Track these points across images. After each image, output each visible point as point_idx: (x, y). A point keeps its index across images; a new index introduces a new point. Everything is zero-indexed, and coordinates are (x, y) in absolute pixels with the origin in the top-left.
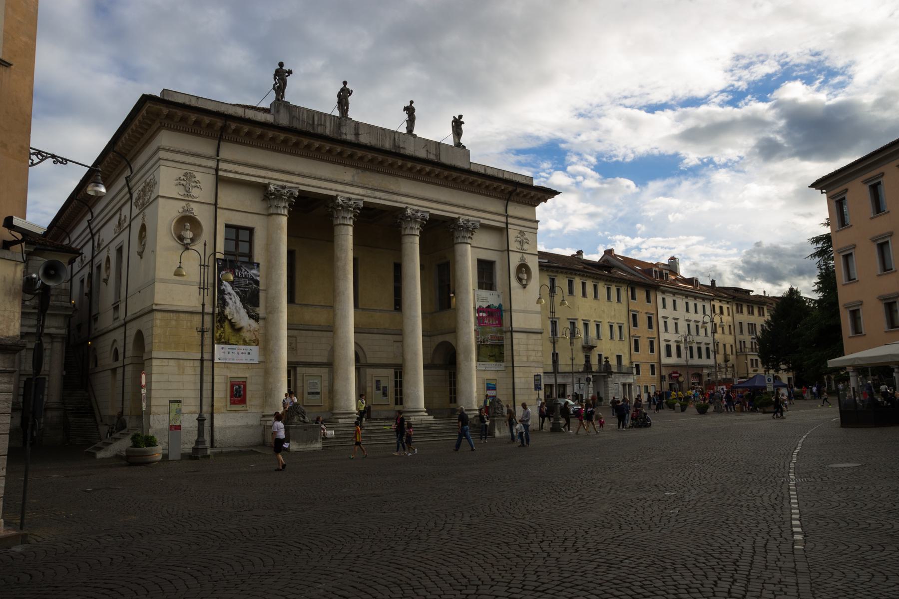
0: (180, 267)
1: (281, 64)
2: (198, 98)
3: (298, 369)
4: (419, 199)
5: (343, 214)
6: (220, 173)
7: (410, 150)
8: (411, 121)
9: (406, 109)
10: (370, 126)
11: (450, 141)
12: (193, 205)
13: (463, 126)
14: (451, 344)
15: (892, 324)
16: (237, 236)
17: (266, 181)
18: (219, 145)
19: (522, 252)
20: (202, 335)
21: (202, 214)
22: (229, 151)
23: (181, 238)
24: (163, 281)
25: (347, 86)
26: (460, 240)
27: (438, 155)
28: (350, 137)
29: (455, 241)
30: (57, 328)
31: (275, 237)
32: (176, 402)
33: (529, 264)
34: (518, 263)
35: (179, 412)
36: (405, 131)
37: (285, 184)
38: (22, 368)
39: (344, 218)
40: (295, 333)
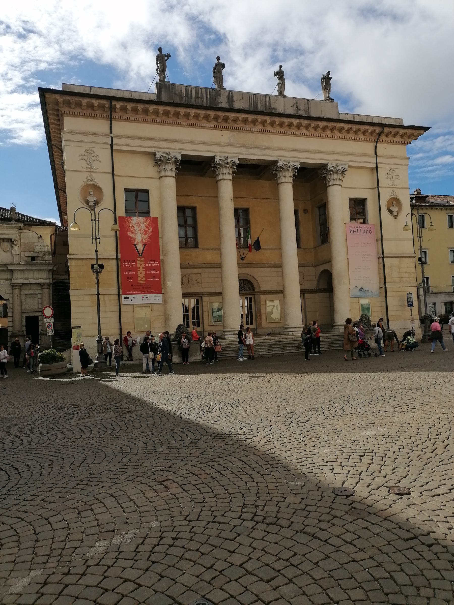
0: (406, 225)
2: (91, 87)
3: (203, 298)
4: (290, 149)
6: (114, 147)
8: (282, 85)
11: (322, 97)
12: (94, 175)
13: (331, 81)
14: (329, 271)
15: (451, 226)
16: (137, 197)
17: (152, 150)
18: (111, 124)
21: (105, 183)
22: (120, 127)
23: (87, 202)
24: (105, 237)
25: (220, 61)
26: (331, 183)
27: (354, 118)
29: (327, 185)
30: (43, 279)
31: (165, 196)
33: (100, 185)
34: (389, 198)
36: (276, 93)
38: (23, 307)
40: (302, 269)
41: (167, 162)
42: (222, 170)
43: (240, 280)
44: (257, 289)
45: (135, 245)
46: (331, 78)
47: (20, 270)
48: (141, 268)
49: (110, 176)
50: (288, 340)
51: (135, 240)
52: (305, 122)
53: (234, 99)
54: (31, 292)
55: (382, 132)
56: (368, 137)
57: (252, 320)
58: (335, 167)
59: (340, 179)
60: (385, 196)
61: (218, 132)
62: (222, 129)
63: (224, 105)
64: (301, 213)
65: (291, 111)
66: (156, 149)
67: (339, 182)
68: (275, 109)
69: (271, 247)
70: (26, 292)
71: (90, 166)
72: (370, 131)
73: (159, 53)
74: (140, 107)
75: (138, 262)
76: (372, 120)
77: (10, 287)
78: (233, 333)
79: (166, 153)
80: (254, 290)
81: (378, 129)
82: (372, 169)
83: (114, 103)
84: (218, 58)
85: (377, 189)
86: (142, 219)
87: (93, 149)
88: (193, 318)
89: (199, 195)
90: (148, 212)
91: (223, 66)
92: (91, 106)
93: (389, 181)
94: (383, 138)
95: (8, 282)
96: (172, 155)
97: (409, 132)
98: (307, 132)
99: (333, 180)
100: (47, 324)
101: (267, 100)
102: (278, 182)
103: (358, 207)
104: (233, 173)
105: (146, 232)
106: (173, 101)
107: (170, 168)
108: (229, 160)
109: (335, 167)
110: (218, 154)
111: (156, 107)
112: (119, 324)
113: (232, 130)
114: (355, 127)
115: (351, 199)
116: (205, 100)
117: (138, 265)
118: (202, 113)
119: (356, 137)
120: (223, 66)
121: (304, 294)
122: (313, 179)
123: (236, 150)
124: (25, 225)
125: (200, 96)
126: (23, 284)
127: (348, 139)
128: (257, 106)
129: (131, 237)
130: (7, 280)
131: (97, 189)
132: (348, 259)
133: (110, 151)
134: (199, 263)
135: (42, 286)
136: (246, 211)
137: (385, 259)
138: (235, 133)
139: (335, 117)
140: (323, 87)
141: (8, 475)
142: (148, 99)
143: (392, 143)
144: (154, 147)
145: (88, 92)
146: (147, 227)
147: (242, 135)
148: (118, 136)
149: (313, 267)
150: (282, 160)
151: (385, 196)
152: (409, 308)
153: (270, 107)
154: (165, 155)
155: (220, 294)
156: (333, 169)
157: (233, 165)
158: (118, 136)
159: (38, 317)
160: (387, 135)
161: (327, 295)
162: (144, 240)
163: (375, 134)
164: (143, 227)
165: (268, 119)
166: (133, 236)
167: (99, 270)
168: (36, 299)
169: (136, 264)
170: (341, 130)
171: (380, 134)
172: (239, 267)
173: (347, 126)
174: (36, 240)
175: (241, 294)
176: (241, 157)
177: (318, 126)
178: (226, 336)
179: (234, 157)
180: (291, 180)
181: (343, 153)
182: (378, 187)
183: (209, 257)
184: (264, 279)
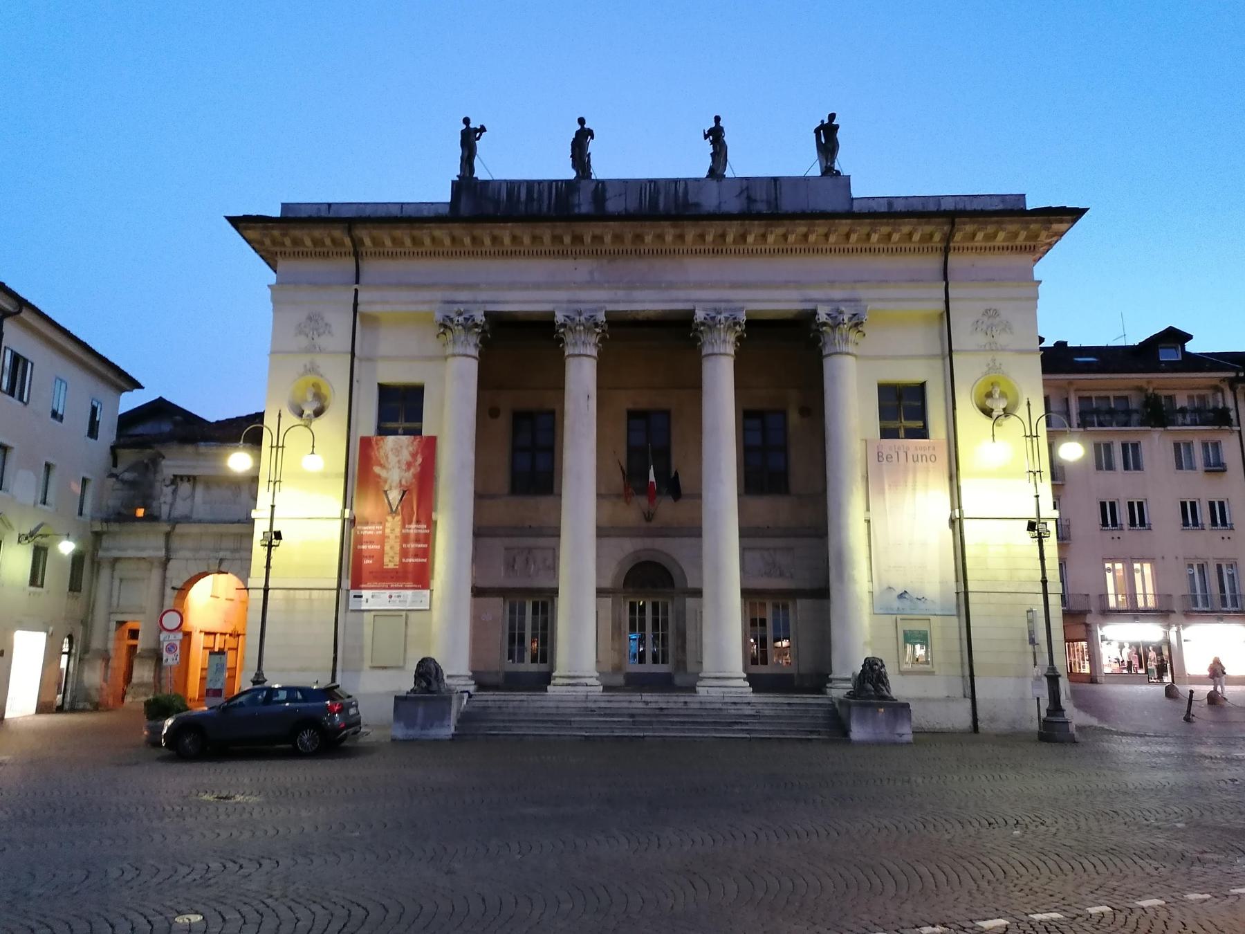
1: (466, 121)
2: (329, 205)
4: (730, 286)
6: (360, 308)
7: (709, 201)
36: (816, 171)
44: (678, 584)
45: (385, 492)
48: (392, 536)
50: (692, 706)
51: (386, 481)
53: (608, 195)
57: (665, 654)
63: (585, 208)
65: (734, 206)
68: (697, 205)
75: (388, 525)
76: (940, 205)
86: (405, 439)
99: (834, 341)
100: (165, 644)
101: (681, 190)
105: (409, 465)
106: (483, 210)
116: (546, 202)
117: (388, 531)
123: (562, 295)
128: (657, 203)
129: (379, 476)
132: (868, 522)
138: (605, 262)
142: (432, 214)
146: (414, 456)
153: (686, 204)
154: (713, 314)
156: (829, 321)
162: (404, 482)
164: (406, 455)
166: (383, 473)
167: (275, 542)
169: (384, 530)
176: (610, 307)
180: (731, 350)
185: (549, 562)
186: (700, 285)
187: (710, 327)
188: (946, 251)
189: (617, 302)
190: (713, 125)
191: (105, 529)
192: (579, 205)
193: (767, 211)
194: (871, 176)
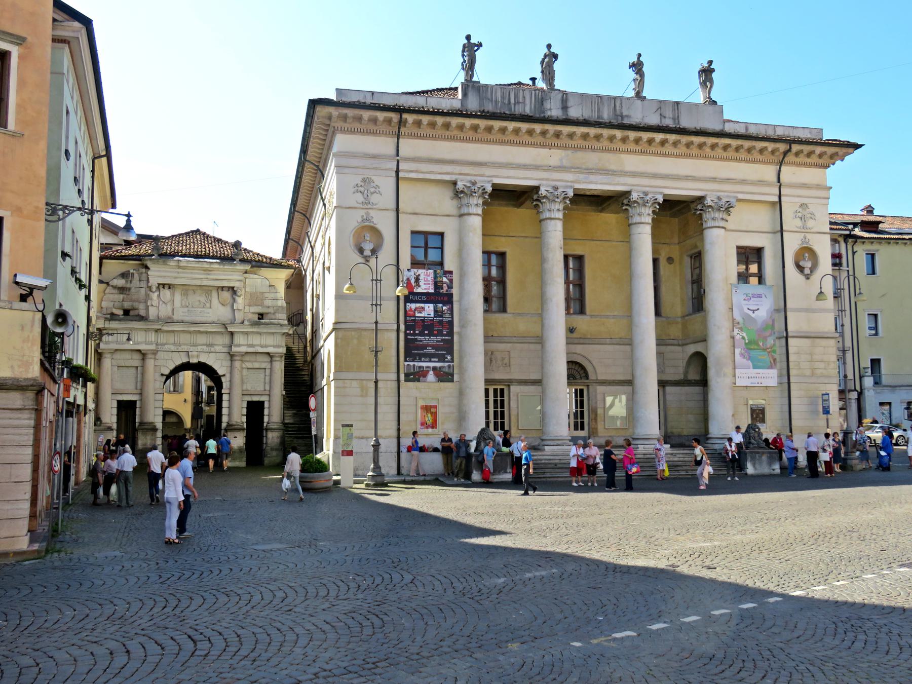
0: (821, 292)
1: (468, 38)
2: (373, 93)
3: (512, 387)
5: (548, 205)
6: (401, 175)
7: (636, 116)
9: (632, 65)
10: (582, 95)
11: (699, 97)
13: (714, 75)
17: (453, 178)
19: (804, 230)
20: (376, 356)
21: (386, 226)
22: (409, 147)
23: (361, 251)
27: (747, 128)
28: (555, 111)
29: (704, 226)
32: (348, 426)
33: (815, 248)
35: (350, 437)
36: (631, 94)
37: (647, 189)
39: (640, 215)
40: (663, 348)
41: (472, 194)
42: (548, 205)
43: (568, 362)
44: (592, 376)
46: (713, 70)
47: (242, 333)
49: (394, 214)
52: (672, 137)
54: (256, 365)
55: (790, 150)
56: (767, 156)
58: (716, 200)
59: (723, 219)
60: (792, 244)
61: (544, 152)
62: (550, 147)
64: (663, 263)
66: (457, 177)
67: (722, 224)
69: (616, 313)
70: (249, 365)
71: (367, 202)
72: (770, 149)
73: (466, 41)
74: (440, 120)
77: (228, 358)
78: (556, 442)
79: (471, 182)
80: (587, 377)
81: (782, 147)
82: (773, 204)
83: (405, 116)
84: (549, 46)
85: (779, 234)
87: (373, 178)
88: (495, 417)
89: (511, 234)
90: (441, 264)
91: (555, 56)
92: (374, 121)
93: (798, 223)
94: (790, 158)
95: (225, 350)
96: (479, 185)
97: (831, 150)
98: (676, 151)
102: (630, 222)
103: (750, 255)
104: (564, 209)
107: (475, 202)
108: (560, 190)
109: (716, 200)
110: (544, 182)
111: (460, 120)
112: (396, 423)
113: (565, 148)
114: (747, 144)
115: (738, 247)
118: (524, 126)
119: (750, 157)
120: (555, 56)
121: (664, 386)
122: (681, 216)
123: (569, 177)
124: (252, 267)
125: (521, 100)
126: (247, 353)
127: (737, 160)
130: (224, 346)
131: (376, 232)
133: (394, 180)
134: (508, 335)
135: (271, 357)
136: (580, 259)
137: (790, 340)
139: (717, 127)
140: (701, 83)
141: (192, 640)
143: (805, 165)
144: (455, 174)
145: (369, 100)
147: (580, 154)
148: (407, 159)
149: (679, 345)
150: (637, 191)
151: (792, 244)
152: (825, 416)
154: (469, 185)
155: (538, 382)
156: (713, 205)
157: (564, 198)
158: (407, 159)
159: (263, 402)
160: (797, 154)
161: (697, 389)
163: (777, 153)
165: (619, 133)
168: (262, 376)
170: (726, 148)
171: (785, 153)
172: (569, 342)
173: (734, 143)
174: (266, 289)
175: (570, 384)
176: (577, 186)
177: (692, 143)
178: (546, 448)
179: (567, 187)
180: (649, 219)
181: (728, 181)
182: (782, 231)
183: (523, 326)
184: (602, 361)
185: (506, 361)
186: (633, 174)
187: (466, 194)
188: (781, 164)
189: (579, 182)
190: (636, 60)
191: (107, 326)
192: (550, 109)
193: (674, 129)
194: (740, 108)
